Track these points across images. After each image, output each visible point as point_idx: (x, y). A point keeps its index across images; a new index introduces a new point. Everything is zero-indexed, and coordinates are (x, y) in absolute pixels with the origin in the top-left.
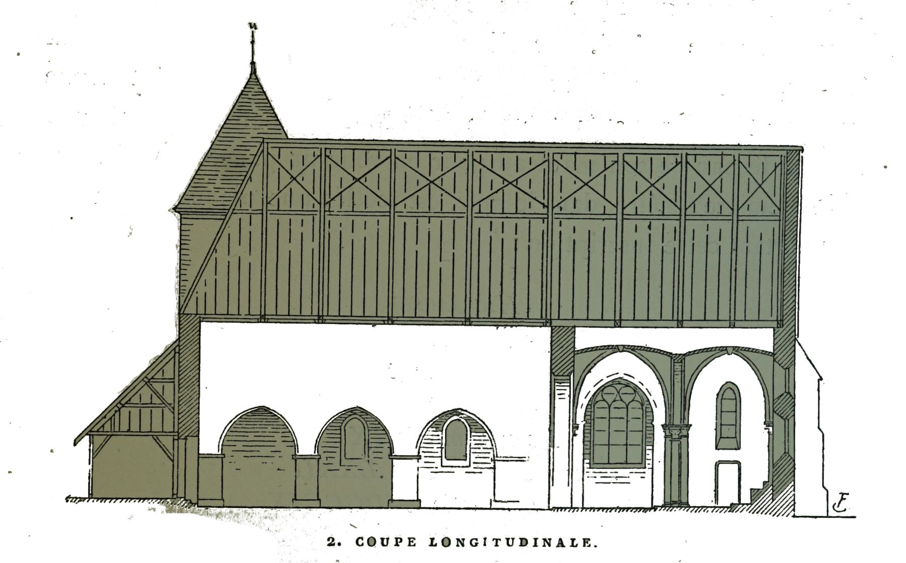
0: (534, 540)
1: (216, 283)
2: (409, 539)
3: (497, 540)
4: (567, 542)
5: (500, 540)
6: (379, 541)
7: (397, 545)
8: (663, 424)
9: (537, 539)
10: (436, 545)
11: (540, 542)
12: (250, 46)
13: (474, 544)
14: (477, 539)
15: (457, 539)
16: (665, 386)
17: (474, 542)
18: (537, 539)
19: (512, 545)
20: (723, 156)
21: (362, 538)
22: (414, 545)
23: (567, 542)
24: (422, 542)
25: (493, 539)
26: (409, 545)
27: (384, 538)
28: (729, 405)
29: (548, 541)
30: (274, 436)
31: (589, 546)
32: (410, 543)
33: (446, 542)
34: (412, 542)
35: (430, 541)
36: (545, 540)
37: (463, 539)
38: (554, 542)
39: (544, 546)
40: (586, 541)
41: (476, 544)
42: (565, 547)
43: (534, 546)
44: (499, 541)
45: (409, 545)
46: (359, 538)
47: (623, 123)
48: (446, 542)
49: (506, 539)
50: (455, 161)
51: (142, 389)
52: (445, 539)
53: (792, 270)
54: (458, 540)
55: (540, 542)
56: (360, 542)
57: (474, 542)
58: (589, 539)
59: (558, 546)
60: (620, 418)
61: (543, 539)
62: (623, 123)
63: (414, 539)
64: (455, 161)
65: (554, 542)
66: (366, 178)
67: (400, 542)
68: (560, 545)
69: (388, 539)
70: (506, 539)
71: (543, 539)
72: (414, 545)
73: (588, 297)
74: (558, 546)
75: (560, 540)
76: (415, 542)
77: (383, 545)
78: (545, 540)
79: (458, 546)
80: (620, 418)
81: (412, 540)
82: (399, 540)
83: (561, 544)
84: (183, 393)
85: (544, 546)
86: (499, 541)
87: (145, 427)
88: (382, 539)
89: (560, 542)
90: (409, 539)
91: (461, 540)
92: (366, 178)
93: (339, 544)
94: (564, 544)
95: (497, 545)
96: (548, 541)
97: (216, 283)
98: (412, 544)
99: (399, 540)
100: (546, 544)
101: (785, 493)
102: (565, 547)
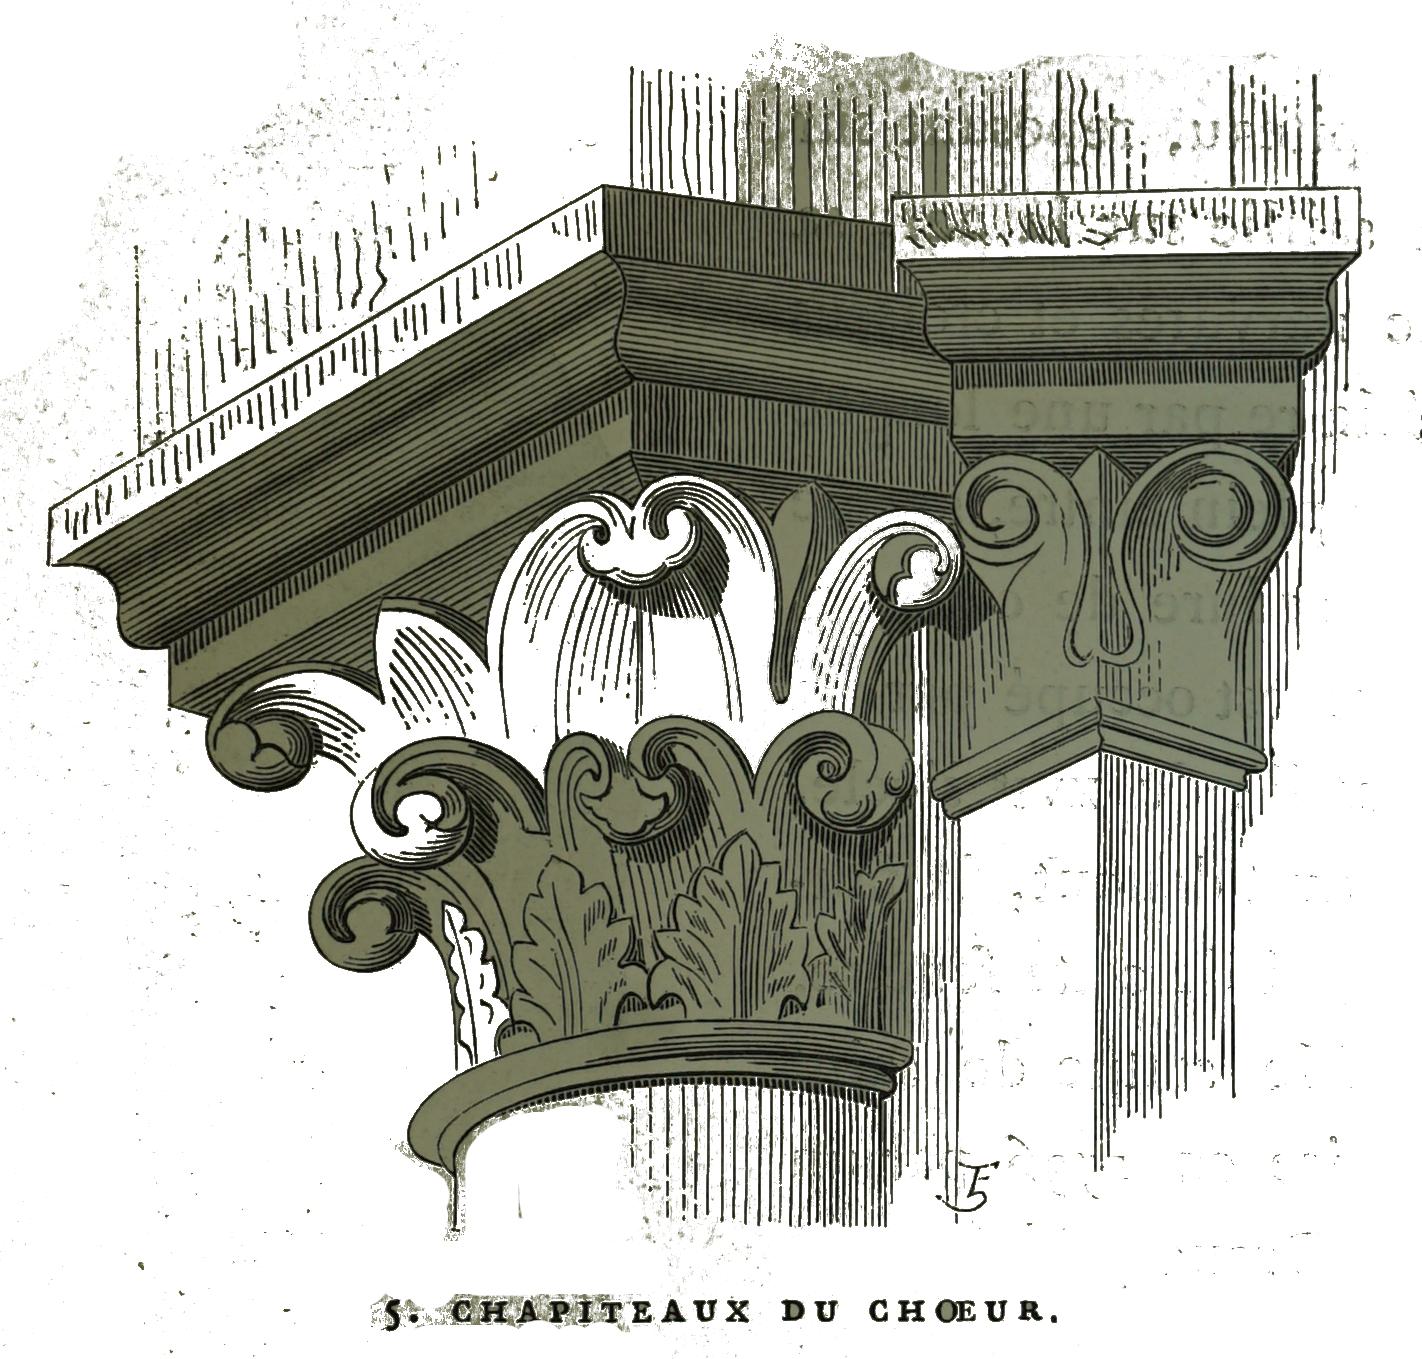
5: (619, 1305)
6: (811, 1311)
16: (492, 939)
19: (831, 1319)
27: (824, 1303)
31: (649, 1319)
32: (637, 1315)
40: (967, 1306)
46: (876, 1303)
47: (491, 180)
48: (911, 1311)
49: (696, 1302)
50: (458, 279)
51: (545, 929)
52: (944, 1305)
53: (366, 628)
56: (880, 1311)
58: (647, 1304)
62: (491, 180)
63: (972, 1303)
64: (458, 279)
66: (371, 309)
67: (564, 1313)
68: (737, 1317)
69: (1003, 1304)
70: (696, 1302)
72: (973, 1319)
75: (673, 1304)
77: (822, 1317)
81: (641, 1307)
82: (560, 1308)
84: (853, 961)
88: (820, 1305)
89: (672, 1310)
92: (371, 309)
94: (683, 1313)
98: (641, 1316)
99: (560, 1308)
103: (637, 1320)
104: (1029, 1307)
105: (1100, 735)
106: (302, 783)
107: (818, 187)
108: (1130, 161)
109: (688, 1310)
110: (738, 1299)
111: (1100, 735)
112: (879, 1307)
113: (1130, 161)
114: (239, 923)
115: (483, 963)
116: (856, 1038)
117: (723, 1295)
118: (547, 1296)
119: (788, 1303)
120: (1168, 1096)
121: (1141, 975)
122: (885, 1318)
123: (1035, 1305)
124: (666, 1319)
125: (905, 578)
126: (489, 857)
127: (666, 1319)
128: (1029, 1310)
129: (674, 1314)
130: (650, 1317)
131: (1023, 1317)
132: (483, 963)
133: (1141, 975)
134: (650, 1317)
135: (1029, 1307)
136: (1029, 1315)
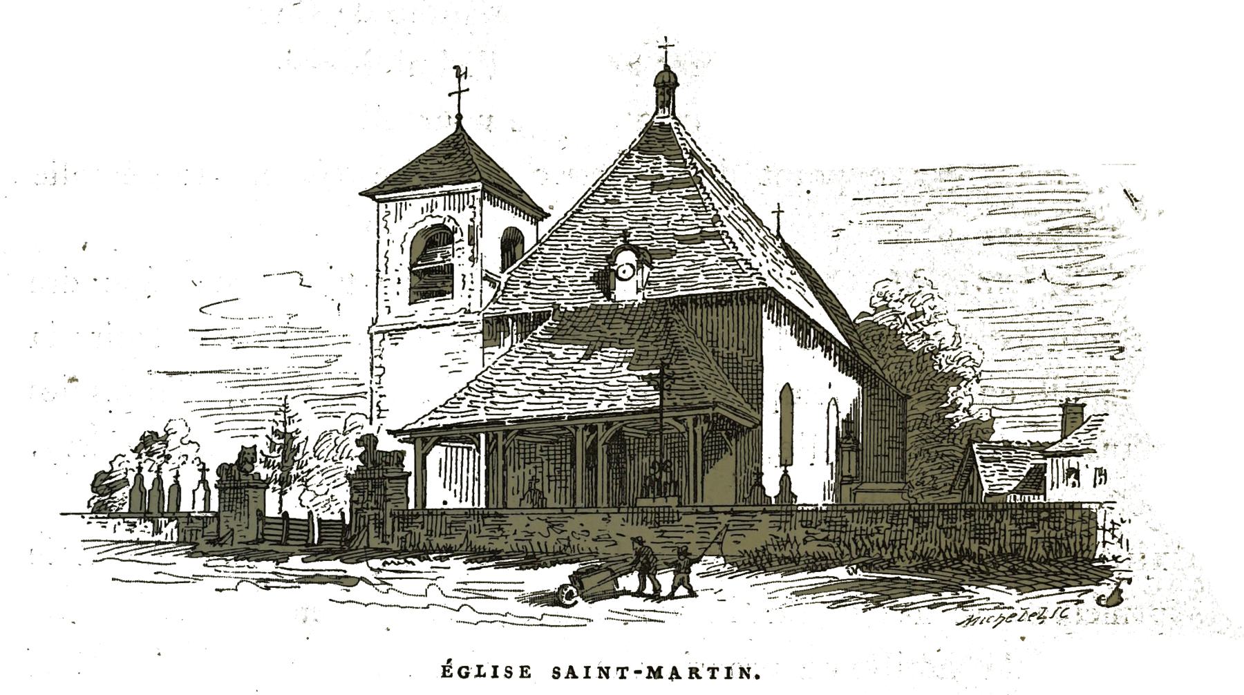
1: (205, 372)
2: (522, 667)
3: (623, 669)
4: (684, 672)
5: (718, 669)
10: (484, 675)
11: (594, 672)
13: (463, 674)
14: (467, 668)
17: (463, 672)
20: (457, 90)
22: (529, 676)
23: (580, 672)
24: (540, 672)
26: (444, 676)
28: (787, 400)
29: (605, 670)
30: (812, 306)
34: (449, 671)
35: (441, 670)
36: (742, 669)
38: (666, 672)
40: (525, 669)
41: (467, 675)
42: (680, 678)
44: (625, 670)
45: (444, 676)
54: (601, 669)
57: (463, 672)
59: (567, 677)
60: (1102, 286)
63: (529, 667)
65: (666, 672)
68: (570, 676)
72: (529, 676)
73: (166, 564)
74: (567, 677)
76: (529, 672)
78: (601, 669)
79: (741, 677)
80: (1102, 286)
83: (675, 674)
89: (674, 672)
90: (522, 667)
93: (757, 677)
94: (680, 674)
95: (713, 677)
96: (605, 670)
97: (205, 372)
98: (447, 674)
100: (603, 675)
102: (680, 678)
103: (522, 676)
104: (694, 671)
108: (240, 430)
109: (684, 672)
113: (240, 429)
114: (460, 73)
115: (788, 384)
117: (737, 663)
120: (650, 600)
122: (451, 676)
123: (697, 670)
124: (671, 678)
125: (246, 448)
126: (805, 347)
127: (476, 676)
128: (744, 672)
130: (452, 674)
131: (691, 677)
132: (788, 384)
134: (452, 674)
135: (694, 671)
136: (694, 676)
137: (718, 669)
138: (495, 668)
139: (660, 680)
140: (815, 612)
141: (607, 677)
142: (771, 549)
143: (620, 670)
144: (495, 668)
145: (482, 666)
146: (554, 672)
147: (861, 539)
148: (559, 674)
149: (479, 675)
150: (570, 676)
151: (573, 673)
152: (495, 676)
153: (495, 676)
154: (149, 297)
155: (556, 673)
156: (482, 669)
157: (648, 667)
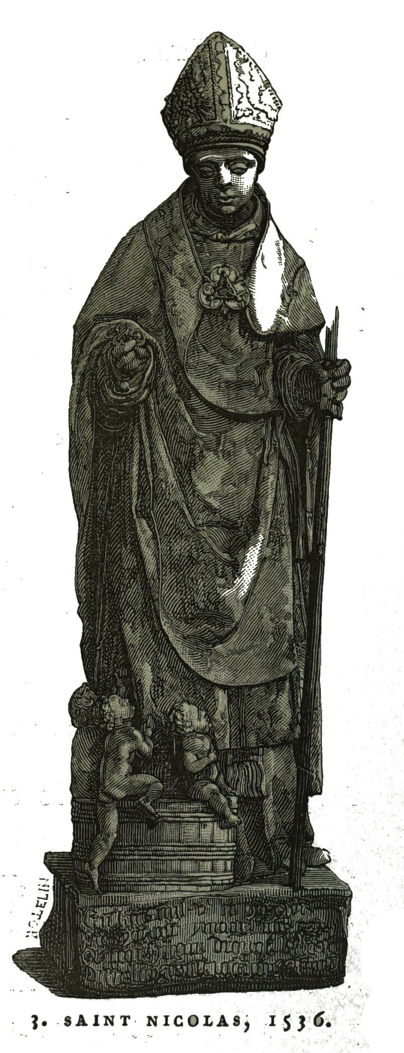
0: (270, 1019)
4: (118, 1022)
5: (129, 1017)
7: (125, 1024)
8: (316, 797)
9: (168, 1016)
11: (161, 1021)
12: (249, 90)
15: (148, 1017)
18: (168, 1016)
21: (181, 1017)
25: (121, 1017)
33: (193, 1021)
36: (107, 1018)
37: (113, 1017)
39: (106, 1024)
43: (164, 1025)
44: (127, 1018)
46: (178, 1017)
55: (161, 1021)
56: (179, 1021)
59: (78, 1025)
61: (105, 1017)
70: (165, 1016)
71: (105, 1017)
74: (78, 1025)
78: (107, 1018)
85: (106, 1024)
86: (127, 1018)
87: (219, 944)
89: (81, 1020)
91: (153, 1017)
94: (86, 1022)
95: (125, 1024)
101: (202, 855)
105: (240, 92)
106: (67, 706)
107: (312, 455)
110: (109, 1015)
111: (240, 92)
112: (179, 1019)
116: (220, 851)
118: (335, 1019)
119: (150, 1018)
121: (230, 510)
122: (181, 1025)
124: (78, 1025)
129: (223, 1022)
133: (230, 510)
137: (129, 1017)
138: (96, 1017)
139: (84, 1027)
140: (34, 894)
141: (112, 1024)
142: (123, 690)
143: (209, 1023)
144: (96, 1017)
145: (209, 1016)
146: (235, 1020)
147: (115, 335)
148: (239, 1022)
149: (206, 1024)
150: (222, 1024)
151: (83, 1021)
152: (96, 1024)
153: (96, 1024)
154: (363, 309)
155: (68, 1021)
156: (209, 1019)
157: (148, 1017)
